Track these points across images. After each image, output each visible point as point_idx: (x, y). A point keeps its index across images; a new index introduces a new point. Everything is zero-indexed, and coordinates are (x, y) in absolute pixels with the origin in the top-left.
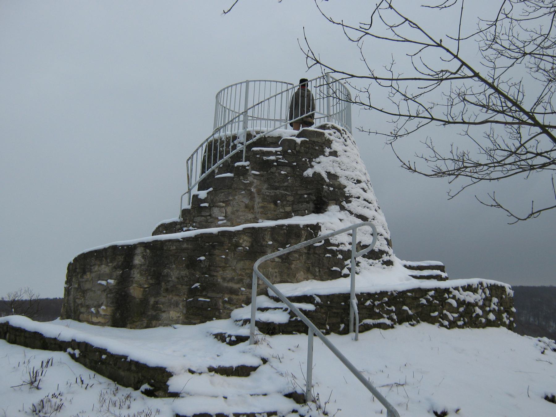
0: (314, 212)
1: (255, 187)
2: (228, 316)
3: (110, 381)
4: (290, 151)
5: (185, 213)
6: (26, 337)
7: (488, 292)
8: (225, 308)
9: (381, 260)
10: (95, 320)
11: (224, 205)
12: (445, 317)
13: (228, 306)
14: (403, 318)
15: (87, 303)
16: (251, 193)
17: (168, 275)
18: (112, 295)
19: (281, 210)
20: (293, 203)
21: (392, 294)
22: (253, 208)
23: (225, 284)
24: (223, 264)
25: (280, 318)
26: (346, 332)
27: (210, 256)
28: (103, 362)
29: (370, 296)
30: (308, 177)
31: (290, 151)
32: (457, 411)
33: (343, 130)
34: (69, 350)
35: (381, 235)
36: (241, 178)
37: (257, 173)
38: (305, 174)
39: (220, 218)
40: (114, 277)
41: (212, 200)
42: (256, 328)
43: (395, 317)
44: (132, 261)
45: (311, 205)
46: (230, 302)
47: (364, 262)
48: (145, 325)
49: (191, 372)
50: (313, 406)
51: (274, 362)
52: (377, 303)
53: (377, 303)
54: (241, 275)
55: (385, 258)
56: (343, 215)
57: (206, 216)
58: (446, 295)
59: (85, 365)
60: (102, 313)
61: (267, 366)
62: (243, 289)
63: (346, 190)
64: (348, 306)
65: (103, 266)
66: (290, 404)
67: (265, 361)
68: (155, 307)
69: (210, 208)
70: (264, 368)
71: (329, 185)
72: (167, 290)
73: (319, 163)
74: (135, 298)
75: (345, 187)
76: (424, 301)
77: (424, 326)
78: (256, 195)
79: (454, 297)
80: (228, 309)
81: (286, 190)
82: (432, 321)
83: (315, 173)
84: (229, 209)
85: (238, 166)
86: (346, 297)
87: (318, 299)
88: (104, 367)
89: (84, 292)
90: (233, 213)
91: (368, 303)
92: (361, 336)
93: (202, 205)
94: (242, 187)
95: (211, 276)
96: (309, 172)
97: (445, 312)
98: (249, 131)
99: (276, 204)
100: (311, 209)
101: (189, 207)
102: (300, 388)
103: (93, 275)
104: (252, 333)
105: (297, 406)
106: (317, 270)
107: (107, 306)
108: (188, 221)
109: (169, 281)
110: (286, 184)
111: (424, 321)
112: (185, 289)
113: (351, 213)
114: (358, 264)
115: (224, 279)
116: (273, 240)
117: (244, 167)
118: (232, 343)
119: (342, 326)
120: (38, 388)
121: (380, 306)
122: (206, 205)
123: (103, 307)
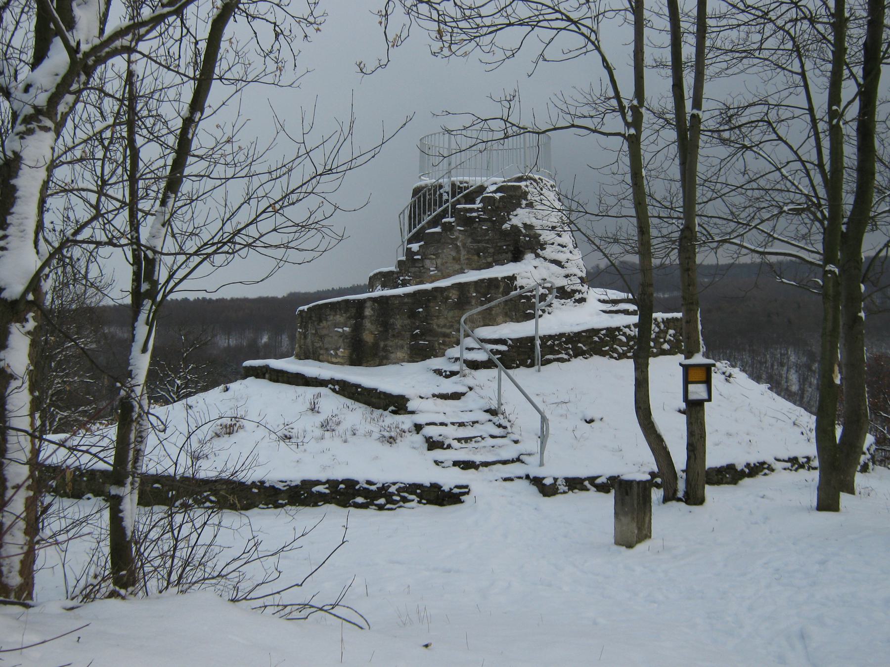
0: (512, 261)
1: (461, 241)
2: (444, 355)
3: (366, 406)
4: (489, 207)
5: (400, 263)
6: (289, 377)
7: (662, 326)
8: (440, 348)
9: (573, 299)
10: (334, 360)
11: (434, 257)
12: (615, 351)
13: (442, 347)
14: (578, 353)
15: (326, 346)
16: (457, 247)
17: (393, 324)
18: (348, 340)
19: (484, 261)
20: (494, 254)
21: (569, 335)
22: (459, 259)
23: (440, 330)
24: (437, 314)
25: (481, 356)
26: (532, 365)
27: (427, 308)
28: (359, 393)
29: (551, 337)
30: (506, 230)
31: (489, 207)
32: (601, 419)
33: (539, 179)
34: (330, 386)
35: (575, 275)
36: (448, 233)
37: (462, 229)
38: (504, 227)
39: (431, 269)
40: (349, 325)
41: (424, 253)
42: (464, 365)
43: (571, 353)
44: (363, 313)
45: (510, 255)
46: (444, 343)
47: (556, 303)
48: (377, 363)
49: (421, 397)
50: (501, 417)
51: (477, 389)
52: (556, 342)
53: (556, 342)
54: (451, 322)
55: (577, 296)
56: (538, 262)
57: (419, 267)
58: (617, 333)
59: (344, 396)
60: (339, 354)
61: (472, 392)
62: (454, 333)
63: (541, 238)
64: (533, 346)
65: (338, 316)
66: (488, 416)
67: (471, 389)
68: (385, 349)
69: (422, 260)
70: (470, 393)
71: (525, 236)
72: (393, 336)
73: (516, 215)
74: (368, 342)
75: (540, 235)
76: (596, 339)
77: (596, 359)
78: (461, 248)
79: (624, 334)
80: (443, 349)
81: (487, 243)
82: (603, 354)
83: (512, 226)
84: (439, 261)
85: (445, 223)
86: (532, 339)
87: (510, 342)
88: (360, 397)
89: (322, 337)
90: (442, 264)
91: (549, 343)
92: (542, 368)
93: (415, 257)
94: (449, 241)
95: (428, 323)
96: (506, 226)
97: (615, 346)
98: (454, 181)
99: (479, 256)
100: (510, 259)
101: (404, 258)
102: (494, 405)
103: (329, 323)
104: (461, 369)
105: (491, 417)
106: (514, 314)
107: (344, 349)
108: (403, 271)
109: (394, 329)
110: (487, 237)
111: (596, 354)
112: (408, 334)
113: (545, 259)
114: (550, 305)
115: (438, 326)
116: (477, 292)
117: (450, 223)
118: (447, 377)
119: (529, 361)
120: (318, 412)
121: (560, 345)
122: (419, 257)
123: (341, 350)
